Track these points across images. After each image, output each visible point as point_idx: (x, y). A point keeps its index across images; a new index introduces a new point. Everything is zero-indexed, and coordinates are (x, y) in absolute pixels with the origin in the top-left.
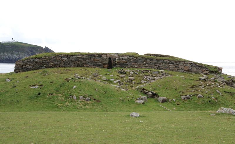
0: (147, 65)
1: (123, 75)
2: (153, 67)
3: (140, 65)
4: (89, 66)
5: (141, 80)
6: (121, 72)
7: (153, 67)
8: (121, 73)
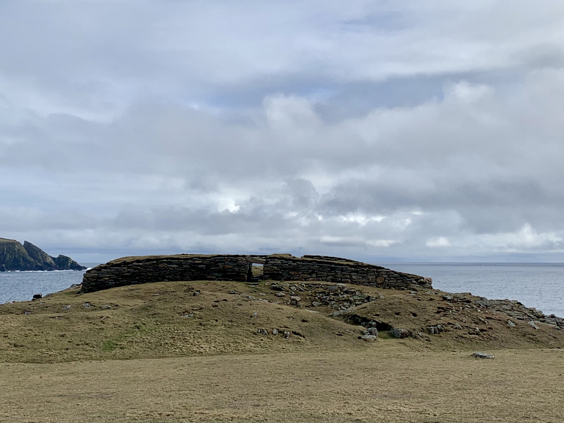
0: (314, 275)
2: (325, 278)
5: (312, 302)
7: (325, 278)
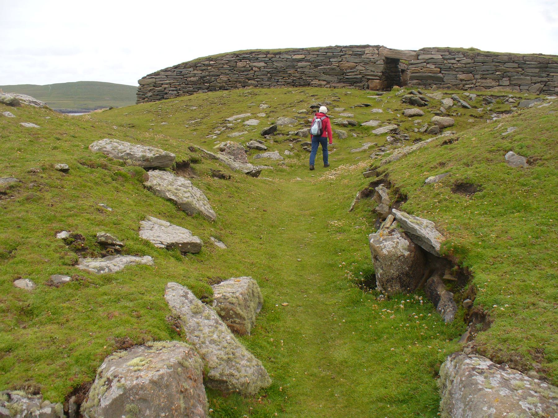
1: (415, 110)
2: (527, 87)
3: (483, 81)
4: (324, 83)
6: (410, 99)
8: (412, 102)
